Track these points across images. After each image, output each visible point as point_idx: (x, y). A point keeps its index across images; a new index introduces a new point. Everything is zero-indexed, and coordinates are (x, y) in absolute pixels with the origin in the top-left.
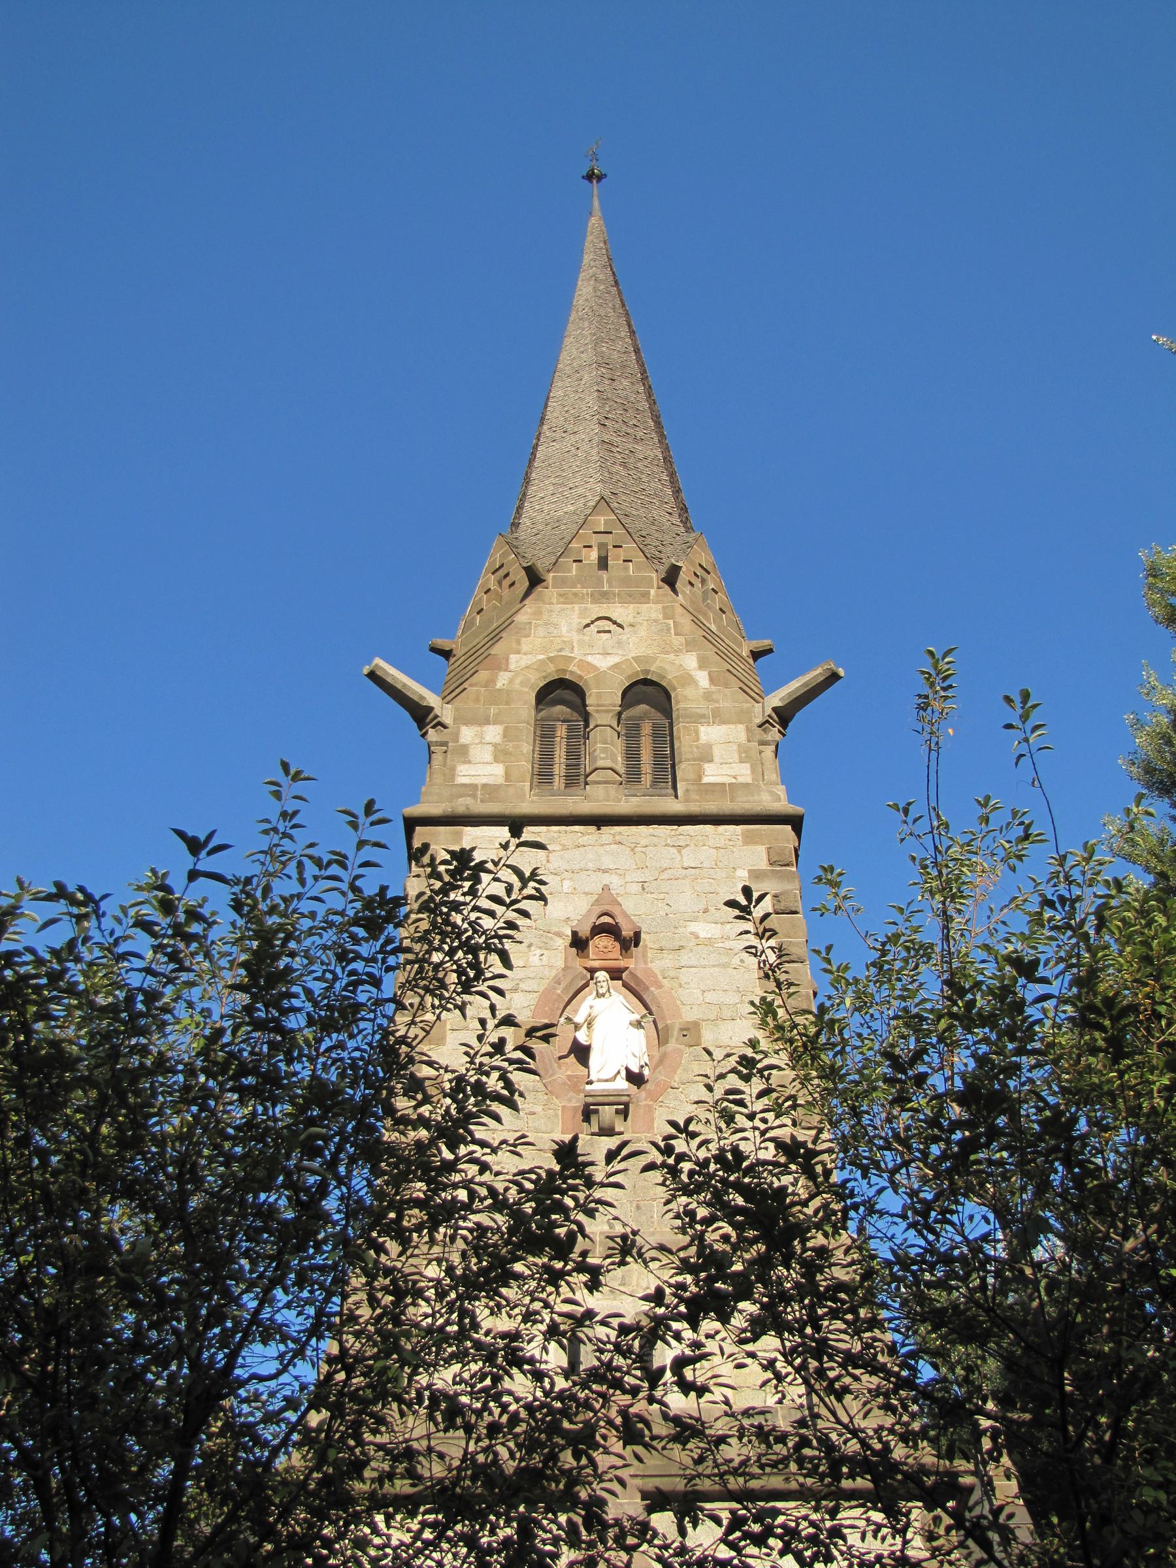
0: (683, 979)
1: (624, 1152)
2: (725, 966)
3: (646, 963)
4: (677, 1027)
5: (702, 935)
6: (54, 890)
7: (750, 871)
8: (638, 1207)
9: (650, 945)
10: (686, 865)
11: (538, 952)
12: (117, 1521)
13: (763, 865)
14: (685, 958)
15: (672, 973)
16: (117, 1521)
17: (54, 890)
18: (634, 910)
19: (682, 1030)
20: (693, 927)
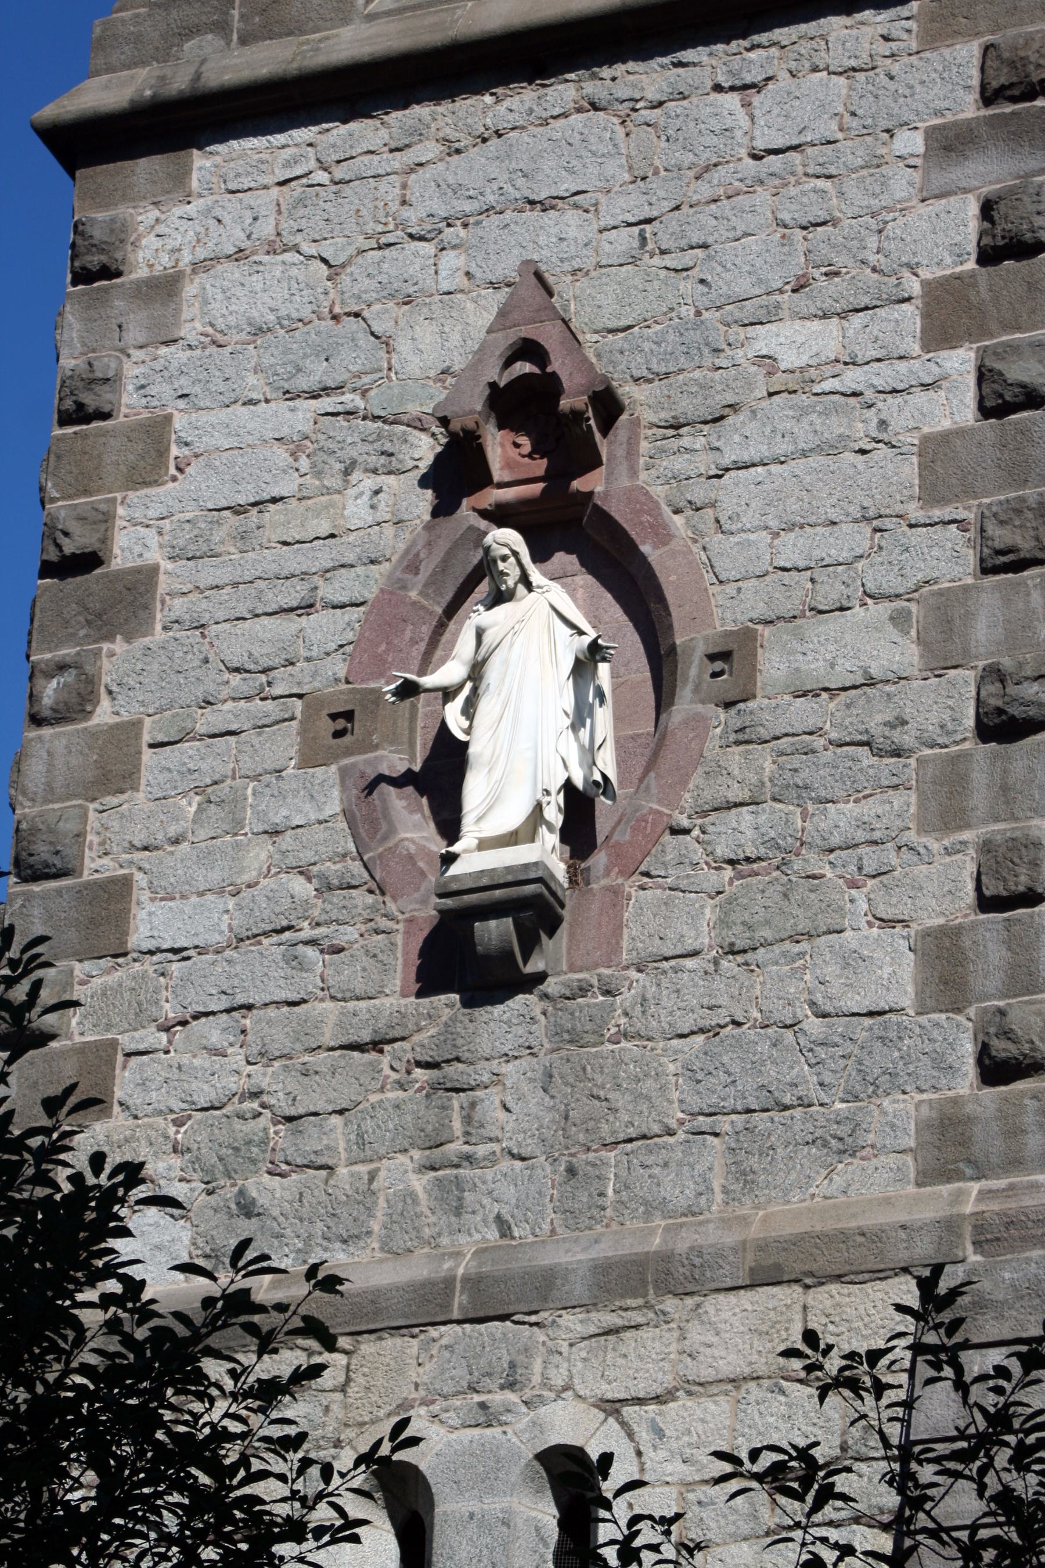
0: (728, 505)
1: (72, 1101)
2: (830, 449)
3: (633, 473)
4: (701, 649)
5: (789, 359)
6: (955, 1433)
7: (930, 134)
8: (571, 1171)
9: (648, 416)
10: (760, 144)
11: (369, 483)
12: (93, 1204)
13: (968, 107)
14: (736, 441)
15: (699, 492)
16: (93, 1204)
17: (955, 1433)
18: (613, 320)
19: (712, 657)
20: (765, 340)
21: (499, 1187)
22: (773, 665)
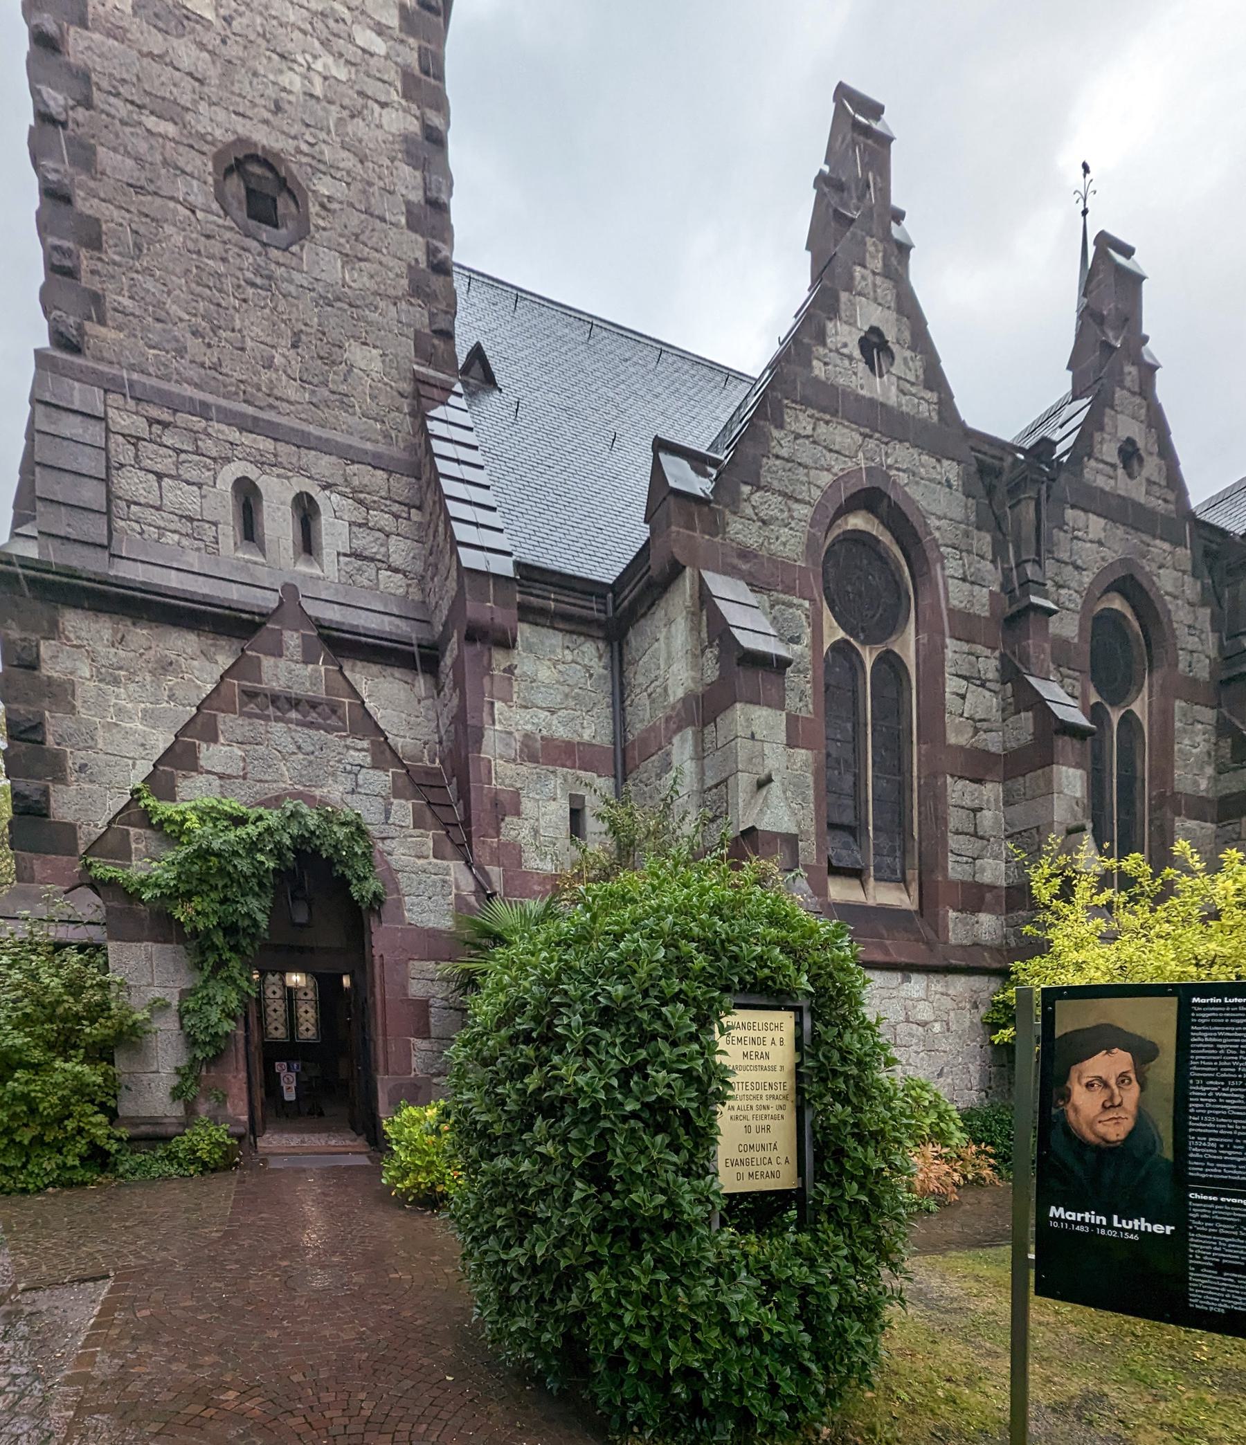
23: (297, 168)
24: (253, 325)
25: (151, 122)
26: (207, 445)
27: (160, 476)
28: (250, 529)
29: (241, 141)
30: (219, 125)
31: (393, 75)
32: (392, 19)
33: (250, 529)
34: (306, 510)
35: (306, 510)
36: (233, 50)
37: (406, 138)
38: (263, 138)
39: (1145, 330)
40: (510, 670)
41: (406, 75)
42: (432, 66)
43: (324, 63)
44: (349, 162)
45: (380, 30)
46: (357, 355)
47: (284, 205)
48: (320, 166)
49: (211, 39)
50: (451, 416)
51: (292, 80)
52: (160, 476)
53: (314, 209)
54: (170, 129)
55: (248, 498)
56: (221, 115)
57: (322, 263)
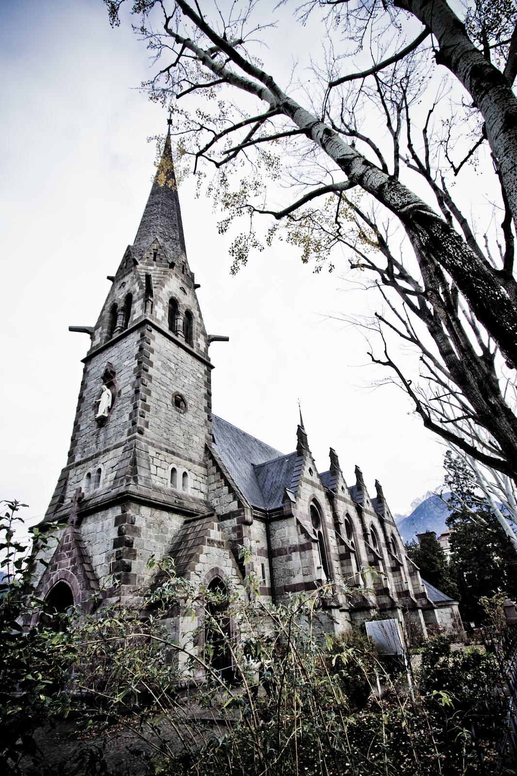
21: (100, 445)
22: (122, 393)
23: (186, 398)
24: (176, 430)
25: (162, 387)
26: (167, 459)
27: (157, 467)
28: (173, 480)
29: (177, 392)
30: (174, 389)
31: (203, 382)
32: (203, 372)
33: (173, 480)
34: (185, 474)
35: (185, 474)
36: (177, 375)
37: (205, 394)
38: (181, 392)
39: (459, 210)
40: (250, 532)
41: (205, 382)
42: (209, 381)
43: (192, 379)
44: (195, 398)
45: (201, 374)
46: (195, 438)
47: (182, 404)
48: (190, 398)
49: (174, 373)
50: (113, 274)
51: (186, 381)
52: (157, 467)
53: (188, 406)
54: (165, 389)
55: (174, 470)
56: (174, 387)
57: (189, 417)
